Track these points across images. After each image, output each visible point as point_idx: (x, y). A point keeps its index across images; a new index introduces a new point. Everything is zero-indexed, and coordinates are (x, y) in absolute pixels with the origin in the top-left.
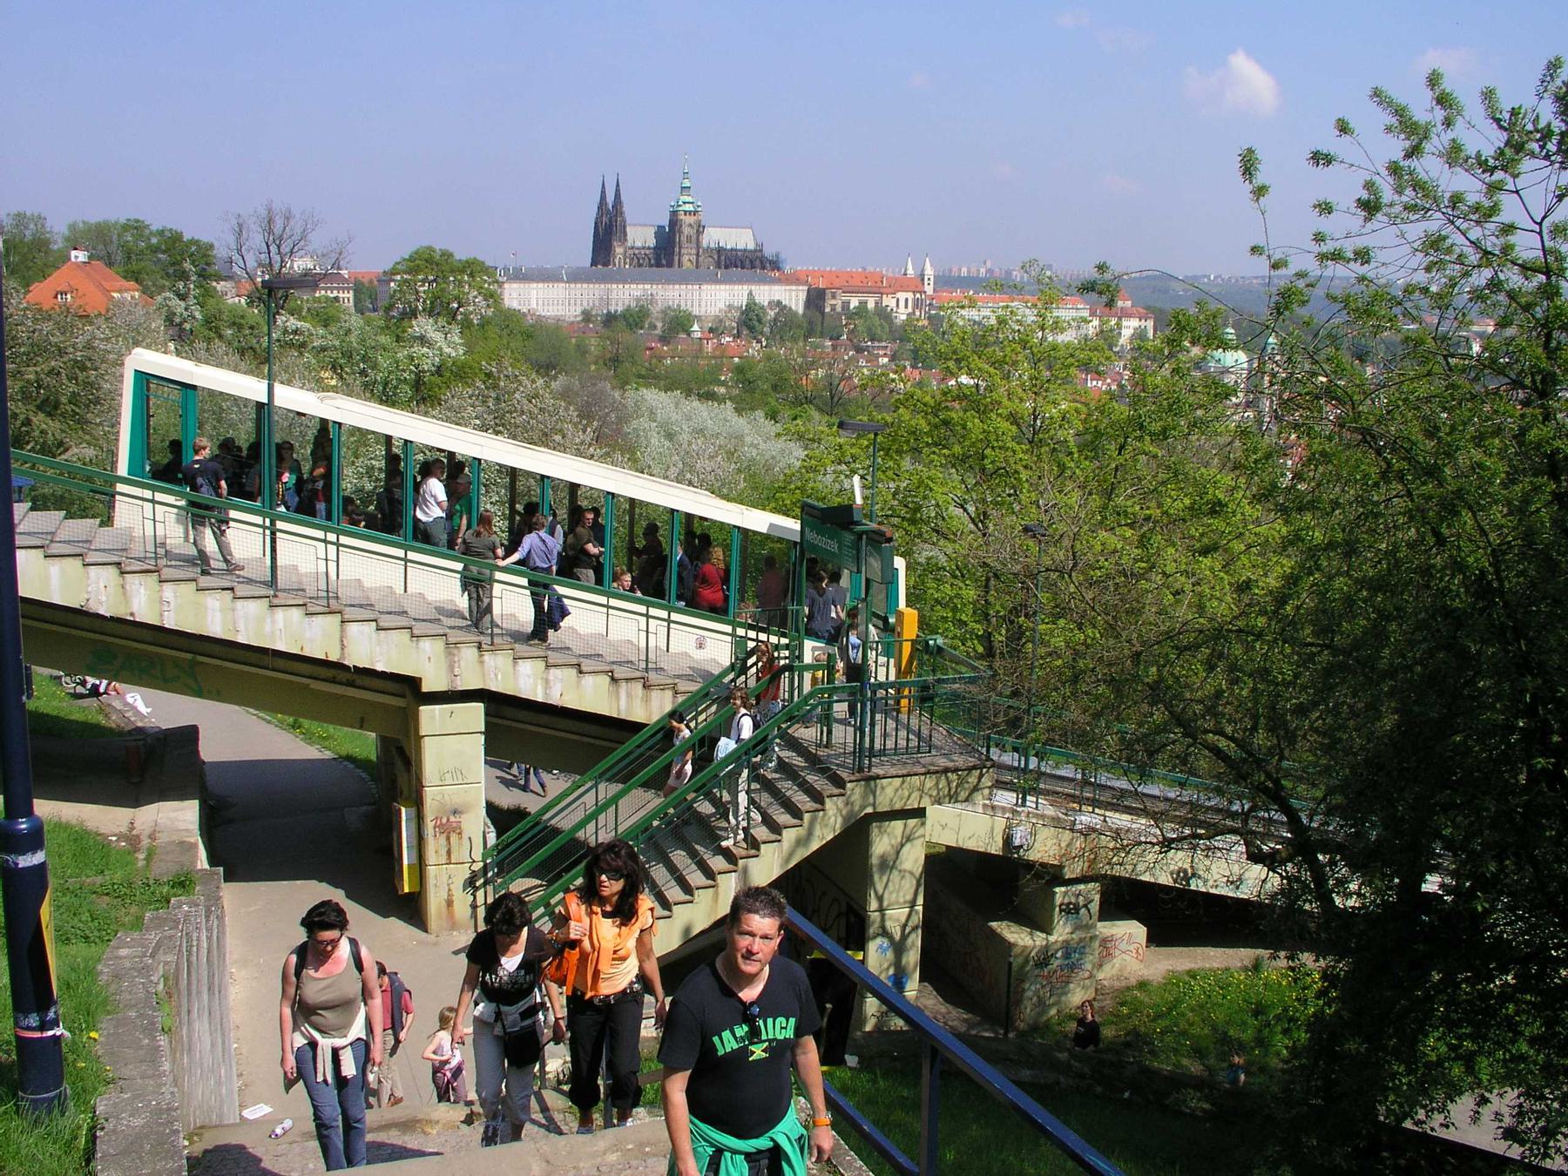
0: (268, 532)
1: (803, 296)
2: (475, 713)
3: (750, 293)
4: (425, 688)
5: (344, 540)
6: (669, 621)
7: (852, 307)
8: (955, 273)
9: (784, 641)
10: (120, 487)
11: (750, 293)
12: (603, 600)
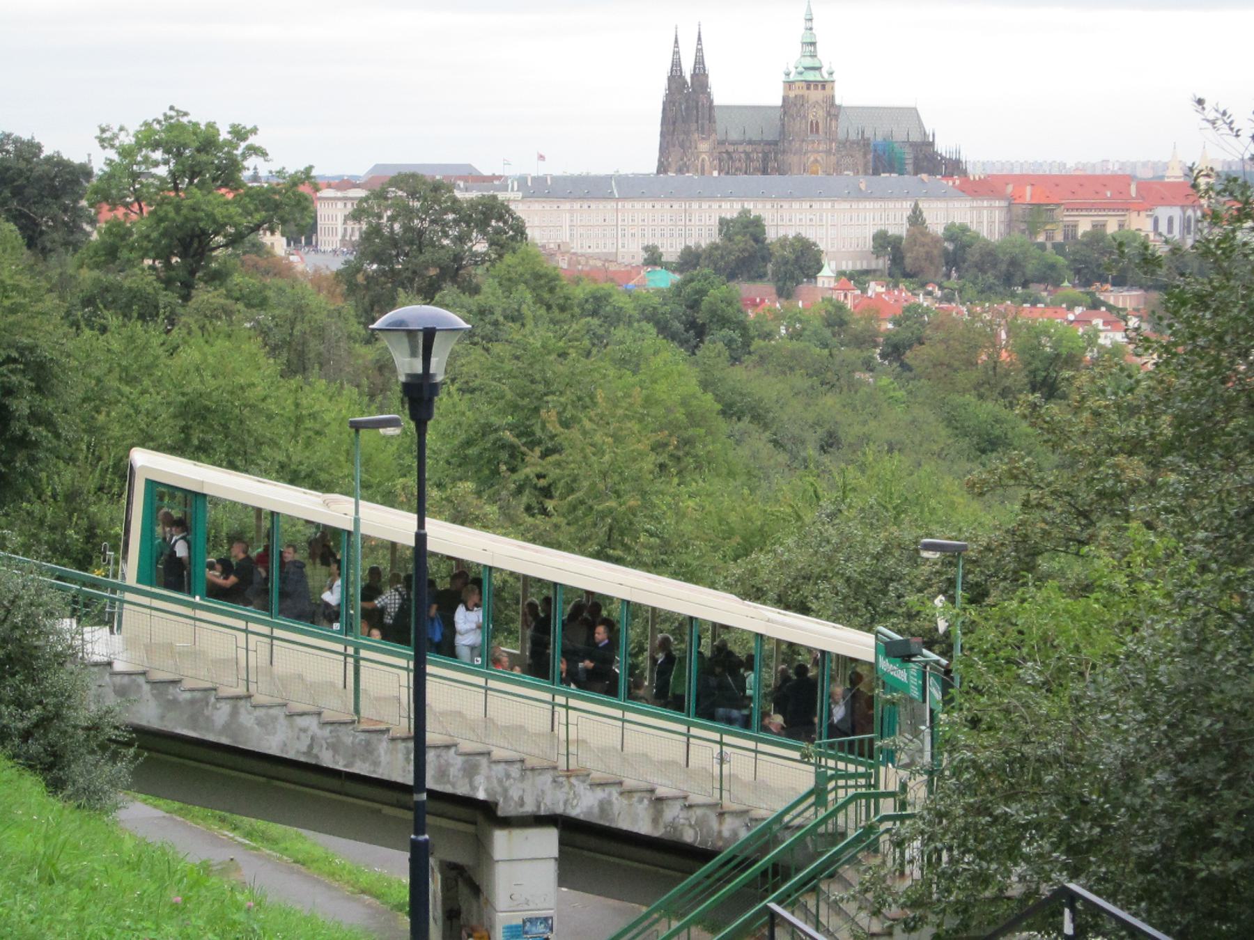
0: (351, 660)
1: (998, 216)
2: (547, 841)
4: (500, 813)
5: (572, 703)
6: (487, 689)
7: (1080, 232)
9: (861, 769)
10: (129, 596)
12: (751, 744)
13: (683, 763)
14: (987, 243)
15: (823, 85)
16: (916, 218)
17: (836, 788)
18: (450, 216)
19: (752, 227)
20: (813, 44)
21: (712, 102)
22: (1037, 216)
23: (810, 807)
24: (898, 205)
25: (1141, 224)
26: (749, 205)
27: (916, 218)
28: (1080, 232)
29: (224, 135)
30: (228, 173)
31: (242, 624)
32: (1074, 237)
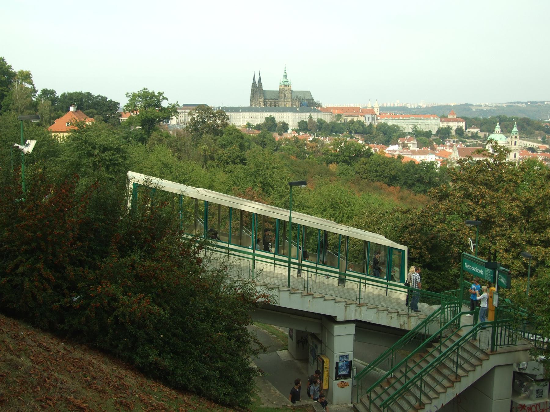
2: (352, 328)
3: (310, 116)
8: (385, 105)
10: (347, 277)
11: (310, 116)
13: (273, 271)
14: (327, 123)
15: (289, 85)
16: (310, 117)
17: (448, 307)
18: (212, 116)
19: (272, 119)
20: (286, 76)
21: (262, 89)
22: (339, 116)
23: (439, 314)
24: (306, 114)
25: (361, 118)
26: (274, 115)
27: (310, 117)
28: (348, 121)
29: (156, 94)
30: (158, 104)
31: (358, 280)
32: (347, 121)
